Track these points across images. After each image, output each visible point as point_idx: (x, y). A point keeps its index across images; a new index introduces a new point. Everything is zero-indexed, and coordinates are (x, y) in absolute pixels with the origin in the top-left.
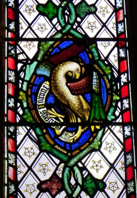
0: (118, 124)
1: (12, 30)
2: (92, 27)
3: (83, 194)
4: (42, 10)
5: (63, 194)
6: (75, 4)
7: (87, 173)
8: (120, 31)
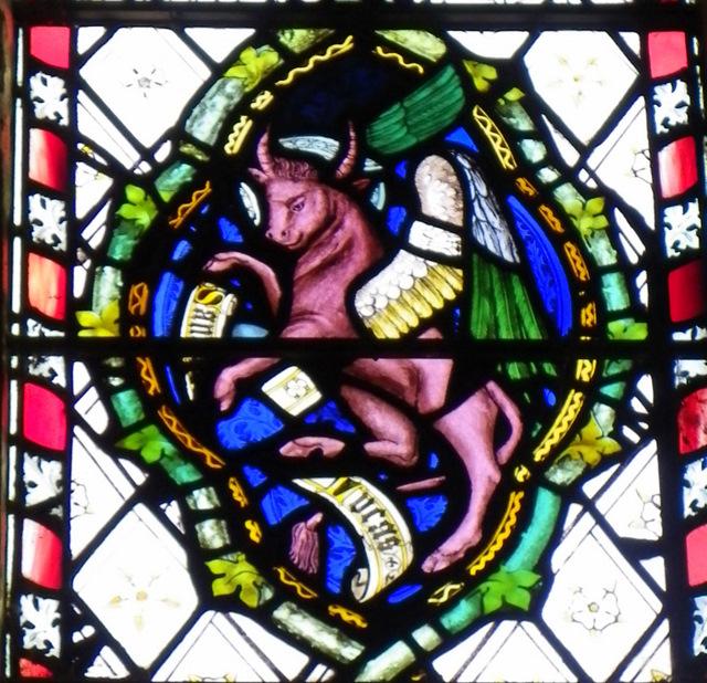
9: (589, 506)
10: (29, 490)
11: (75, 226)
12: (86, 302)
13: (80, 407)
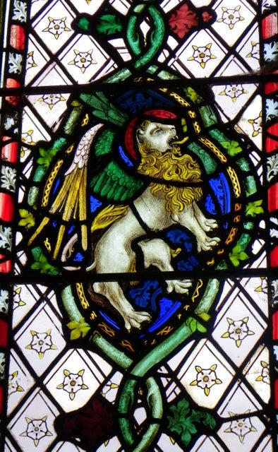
0: (258, 273)
1: (4, 247)
2: (202, 57)
3: (165, 441)
4: (86, 25)
5: (115, 443)
6: (166, 10)
7: (178, 391)
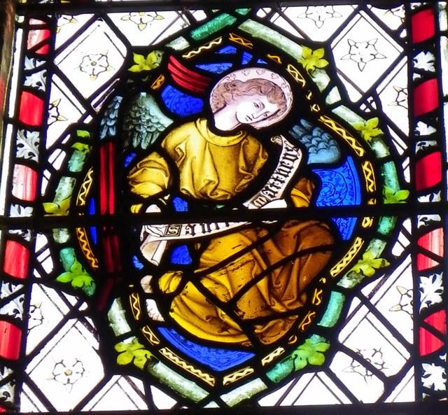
8: (429, 302)
9: (365, 301)
10: (18, 148)
11: (45, 153)
12: (51, 196)
13: (40, 258)
